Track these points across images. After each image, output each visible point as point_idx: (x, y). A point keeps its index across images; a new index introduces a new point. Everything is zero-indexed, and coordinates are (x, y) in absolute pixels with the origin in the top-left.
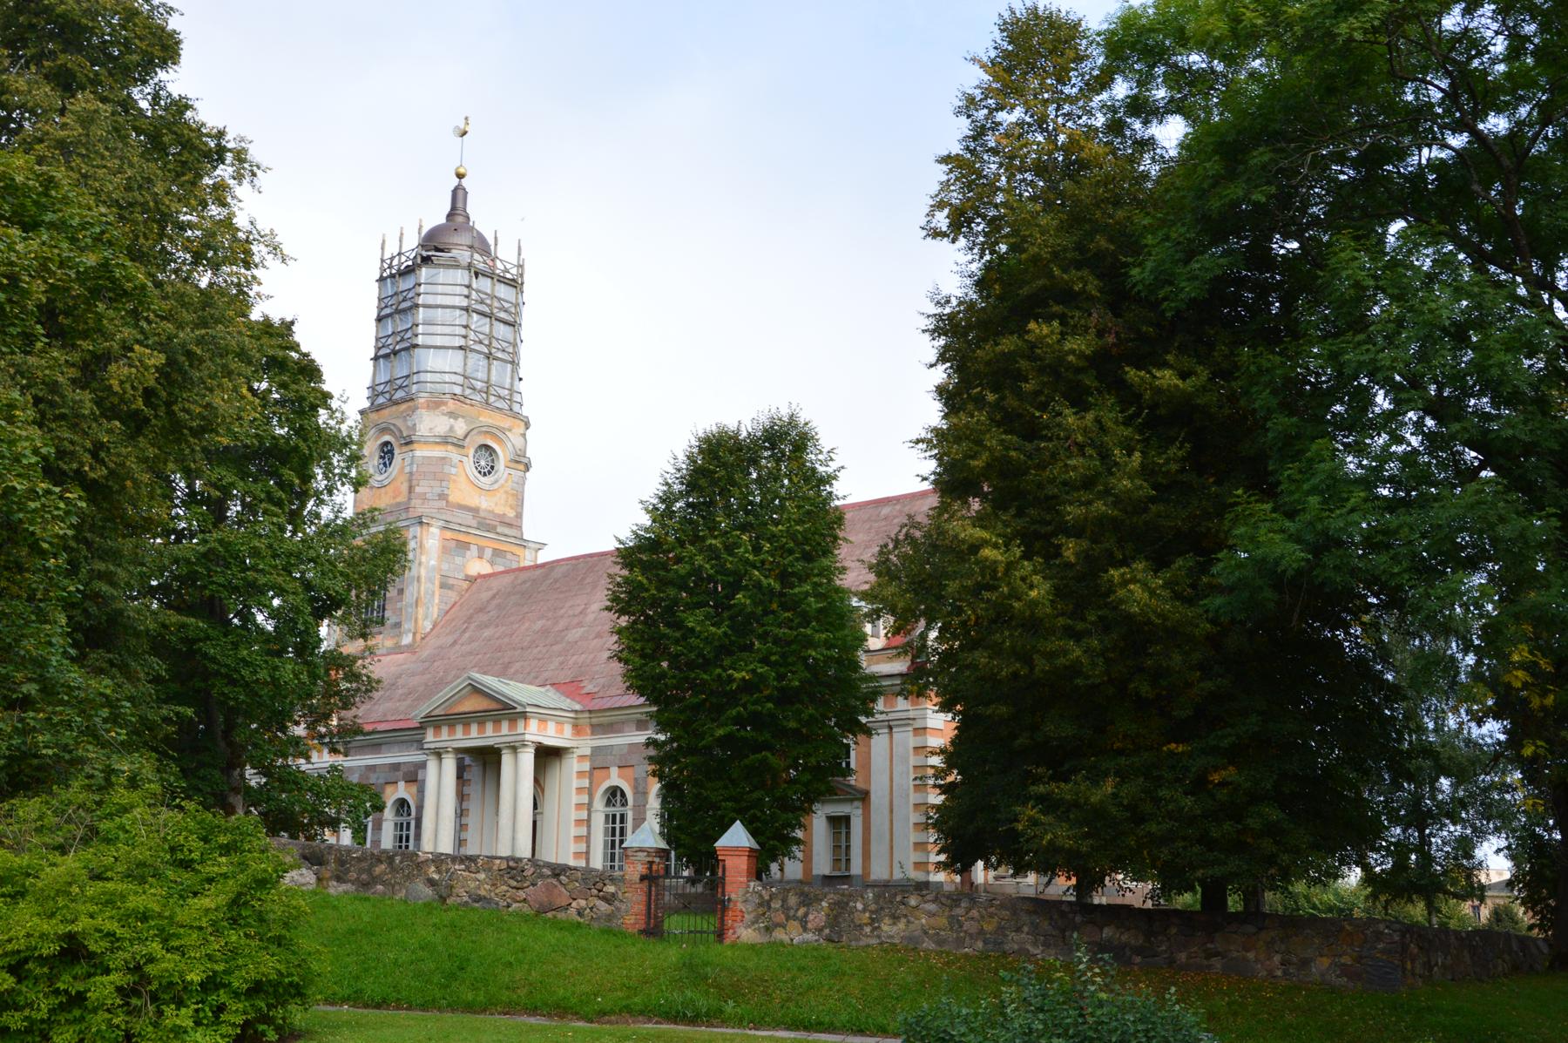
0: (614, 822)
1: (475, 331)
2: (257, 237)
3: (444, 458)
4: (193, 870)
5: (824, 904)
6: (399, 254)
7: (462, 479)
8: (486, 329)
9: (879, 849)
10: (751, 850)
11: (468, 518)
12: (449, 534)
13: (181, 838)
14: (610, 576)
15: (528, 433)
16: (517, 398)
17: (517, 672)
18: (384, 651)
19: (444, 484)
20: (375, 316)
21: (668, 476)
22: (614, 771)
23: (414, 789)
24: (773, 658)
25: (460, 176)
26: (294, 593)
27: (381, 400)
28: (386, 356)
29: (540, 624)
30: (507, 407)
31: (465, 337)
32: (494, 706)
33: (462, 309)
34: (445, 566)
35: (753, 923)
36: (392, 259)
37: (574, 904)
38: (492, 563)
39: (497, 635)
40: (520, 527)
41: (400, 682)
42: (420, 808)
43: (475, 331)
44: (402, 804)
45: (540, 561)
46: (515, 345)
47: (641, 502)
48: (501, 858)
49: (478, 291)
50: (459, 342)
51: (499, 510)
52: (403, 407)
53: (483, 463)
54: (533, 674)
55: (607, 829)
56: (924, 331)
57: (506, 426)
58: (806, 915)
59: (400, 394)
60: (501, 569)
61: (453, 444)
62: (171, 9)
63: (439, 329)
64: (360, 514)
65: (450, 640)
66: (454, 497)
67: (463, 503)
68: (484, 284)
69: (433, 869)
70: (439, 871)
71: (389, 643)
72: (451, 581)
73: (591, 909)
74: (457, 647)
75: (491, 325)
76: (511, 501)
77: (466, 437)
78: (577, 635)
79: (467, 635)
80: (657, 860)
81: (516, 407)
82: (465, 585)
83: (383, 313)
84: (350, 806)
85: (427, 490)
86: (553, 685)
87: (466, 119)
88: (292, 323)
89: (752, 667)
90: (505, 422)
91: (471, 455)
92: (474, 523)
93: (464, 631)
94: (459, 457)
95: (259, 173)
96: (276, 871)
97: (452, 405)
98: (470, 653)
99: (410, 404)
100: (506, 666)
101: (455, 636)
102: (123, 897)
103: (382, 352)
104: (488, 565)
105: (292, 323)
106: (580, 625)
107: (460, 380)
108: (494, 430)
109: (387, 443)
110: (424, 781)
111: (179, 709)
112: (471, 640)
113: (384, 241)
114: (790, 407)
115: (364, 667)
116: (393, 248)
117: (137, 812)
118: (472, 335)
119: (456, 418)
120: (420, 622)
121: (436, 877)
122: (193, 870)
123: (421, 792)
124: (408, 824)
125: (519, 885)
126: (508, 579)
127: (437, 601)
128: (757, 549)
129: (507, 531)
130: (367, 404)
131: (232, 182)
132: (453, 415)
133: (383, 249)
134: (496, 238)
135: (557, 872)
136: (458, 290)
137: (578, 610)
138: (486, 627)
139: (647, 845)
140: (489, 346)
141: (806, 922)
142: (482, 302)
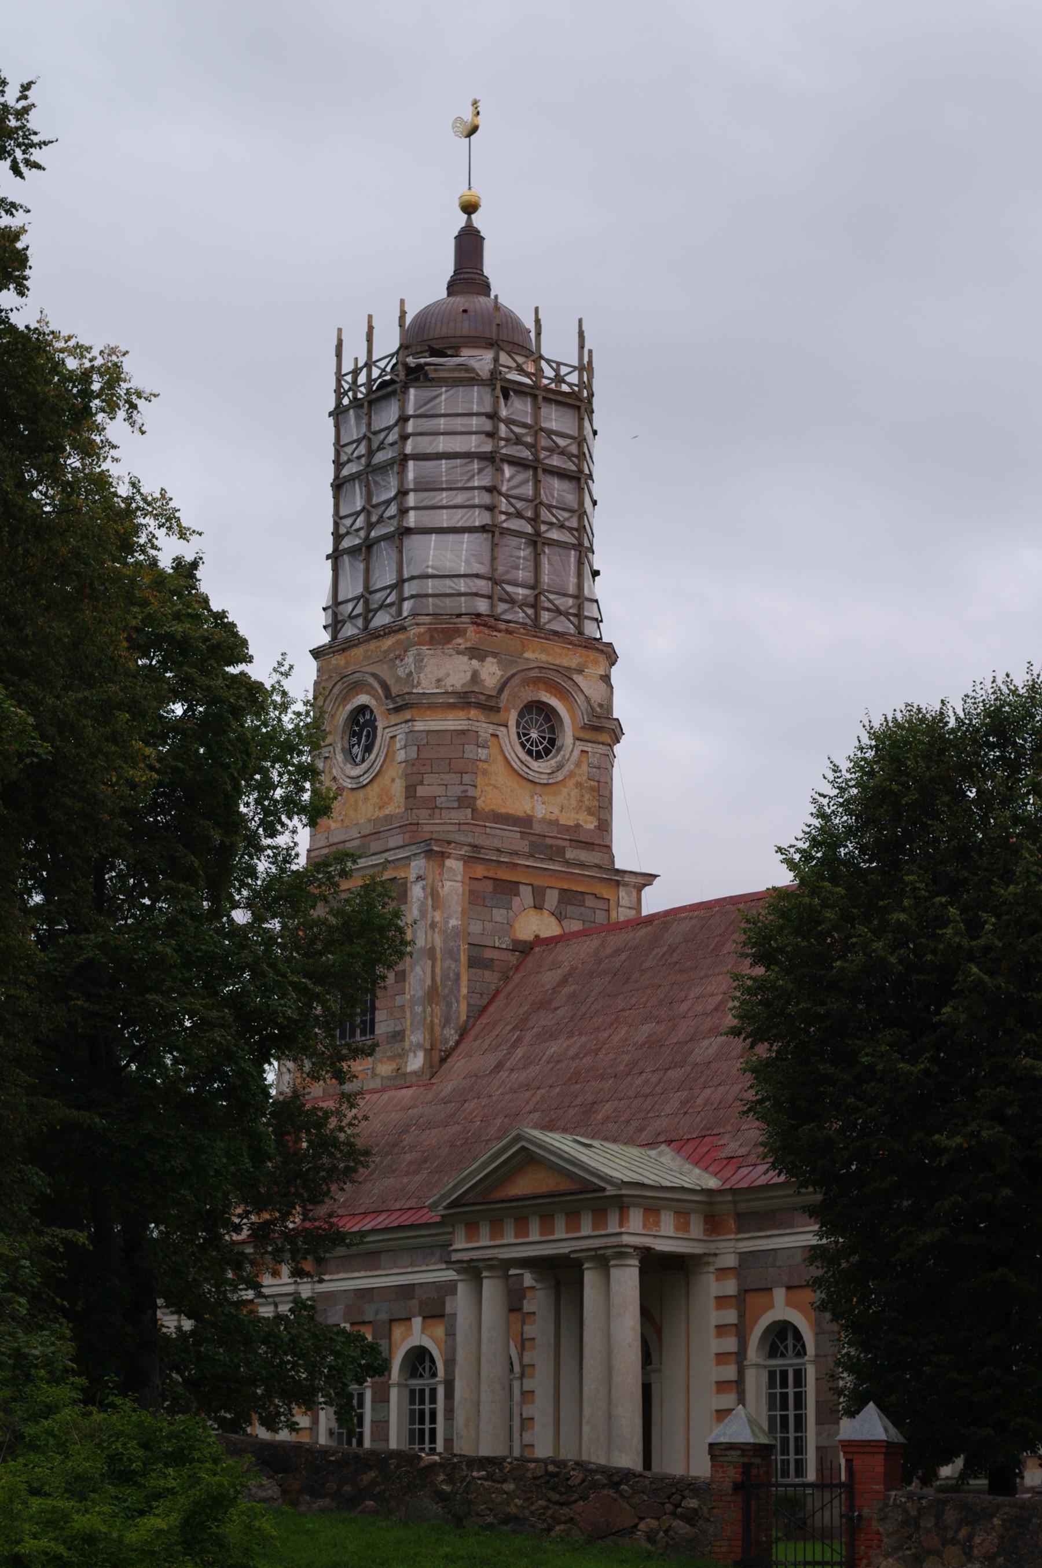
0: (784, 1384)
1: (507, 496)
2: (141, 504)
3: (463, 732)
4: (136, 1483)
5: (996, 1521)
6: (369, 365)
7: (498, 768)
8: (528, 490)
10: (888, 1445)
11: (511, 838)
12: (480, 871)
13: (119, 1445)
14: (736, 977)
15: (615, 672)
16: (590, 610)
17: (606, 1120)
18: (376, 1084)
19: (467, 778)
20: (330, 477)
21: (825, 801)
22: (779, 1294)
23: (440, 1331)
24: (1009, 1112)
25: (469, 208)
26: (222, 1026)
27: (349, 630)
28: (353, 551)
29: (646, 1029)
30: (572, 630)
31: (491, 508)
32: (566, 1185)
33: (482, 457)
34: (476, 928)
35: (896, 1550)
36: (356, 372)
37: (642, 1526)
38: (559, 916)
39: (572, 1052)
41: (408, 1139)
42: (450, 1363)
43: (507, 496)
44: (419, 1359)
45: (645, 911)
46: (581, 514)
47: (780, 850)
48: (536, 1461)
49: (509, 422)
50: (480, 518)
52: (389, 642)
53: (534, 735)
54: (635, 1124)
55: (771, 1397)
57: (573, 664)
58: (970, 1537)
59: (382, 619)
60: (576, 926)
61: (479, 706)
62: (13, 205)
63: (444, 497)
64: (318, 864)
65: (491, 1060)
66: (488, 800)
67: (502, 810)
68: (520, 408)
69: (442, 1477)
70: (450, 1480)
71: (385, 1069)
72: (488, 954)
73: (666, 1531)
74: (503, 1074)
75: (537, 483)
76: (588, 800)
77: (501, 690)
79: (519, 1053)
80: (757, 1461)
81: (590, 629)
82: (513, 959)
83: (345, 472)
84: (331, 1368)
85: (438, 791)
86: (669, 1142)
87: (475, 103)
88: (194, 565)
89: (973, 1127)
90: (571, 659)
91: (512, 723)
92: (523, 846)
93: (515, 1045)
95: (141, 403)
96: (234, 1486)
97: (472, 635)
98: (528, 1086)
99: (401, 636)
100: (589, 1109)
101: (500, 1055)
102: (65, 1517)
103: (346, 543)
105: (194, 565)
107: (483, 586)
108: (552, 675)
109: (363, 709)
110: (454, 1315)
111: (65, 1233)
113: (371, 328)
114: (1029, 671)
115: (341, 1129)
116: (355, 352)
117: (67, 1413)
118: (503, 504)
119: (482, 659)
120: (438, 1029)
121: (446, 1488)
122: (136, 1483)
123: (451, 1333)
124: (433, 1391)
125: (563, 1499)
126: (587, 947)
127: (464, 991)
128: (974, 928)
129: (583, 856)
130: (324, 638)
131: (147, 610)
132: (476, 653)
133: (339, 354)
134: (538, 321)
135: (616, 1479)
136: (474, 423)
138: (553, 1036)
139: (741, 1439)
140: (535, 520)
141: (971, 1547)
142: (518, 441)
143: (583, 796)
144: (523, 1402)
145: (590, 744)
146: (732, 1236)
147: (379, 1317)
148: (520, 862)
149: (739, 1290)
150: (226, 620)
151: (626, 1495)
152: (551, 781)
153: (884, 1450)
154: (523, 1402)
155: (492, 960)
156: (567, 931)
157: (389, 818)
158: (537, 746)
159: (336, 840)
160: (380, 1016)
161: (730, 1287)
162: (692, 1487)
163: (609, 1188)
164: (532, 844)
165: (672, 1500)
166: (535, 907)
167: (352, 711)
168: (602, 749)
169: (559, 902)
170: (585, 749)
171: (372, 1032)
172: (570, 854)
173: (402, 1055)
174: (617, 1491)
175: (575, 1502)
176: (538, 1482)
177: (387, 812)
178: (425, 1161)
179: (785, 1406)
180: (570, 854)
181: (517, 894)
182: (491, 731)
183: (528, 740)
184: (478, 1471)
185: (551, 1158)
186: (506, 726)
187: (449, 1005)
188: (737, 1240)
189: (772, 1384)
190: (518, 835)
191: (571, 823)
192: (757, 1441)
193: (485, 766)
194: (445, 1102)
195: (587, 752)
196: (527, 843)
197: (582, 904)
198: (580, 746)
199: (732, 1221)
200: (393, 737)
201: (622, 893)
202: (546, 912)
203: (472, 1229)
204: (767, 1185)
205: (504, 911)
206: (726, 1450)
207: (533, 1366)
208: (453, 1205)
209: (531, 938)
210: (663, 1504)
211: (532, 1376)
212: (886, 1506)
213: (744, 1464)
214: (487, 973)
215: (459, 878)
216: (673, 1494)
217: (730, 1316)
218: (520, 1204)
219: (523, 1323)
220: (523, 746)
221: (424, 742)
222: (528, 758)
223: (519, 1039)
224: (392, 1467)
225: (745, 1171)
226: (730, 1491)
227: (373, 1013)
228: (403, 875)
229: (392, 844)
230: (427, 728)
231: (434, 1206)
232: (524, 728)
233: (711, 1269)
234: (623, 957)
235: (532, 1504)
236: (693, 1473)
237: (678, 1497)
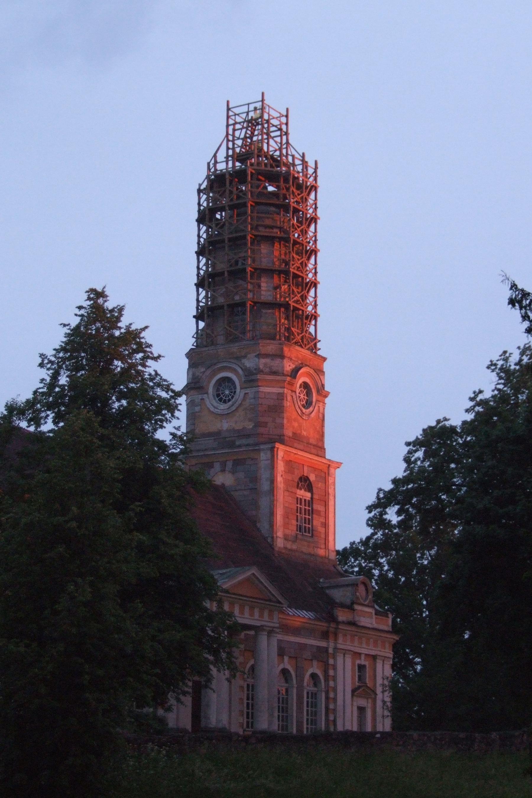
38: (233, 472)
51: (238, 427)
94: (200, 397)
145: (248, 389)
148: (209, 453)
150: (131, 329)
158: (224, 396)
169: (233, 465)
170: (246, 392)
172: (238, 443)
180: (238, 443)
182: (200, 398)
183: (231, 389)
191: (241, 428)
195: (248, 393)
196: (217, 443)
198: (244, 391)
202: (227, 472)
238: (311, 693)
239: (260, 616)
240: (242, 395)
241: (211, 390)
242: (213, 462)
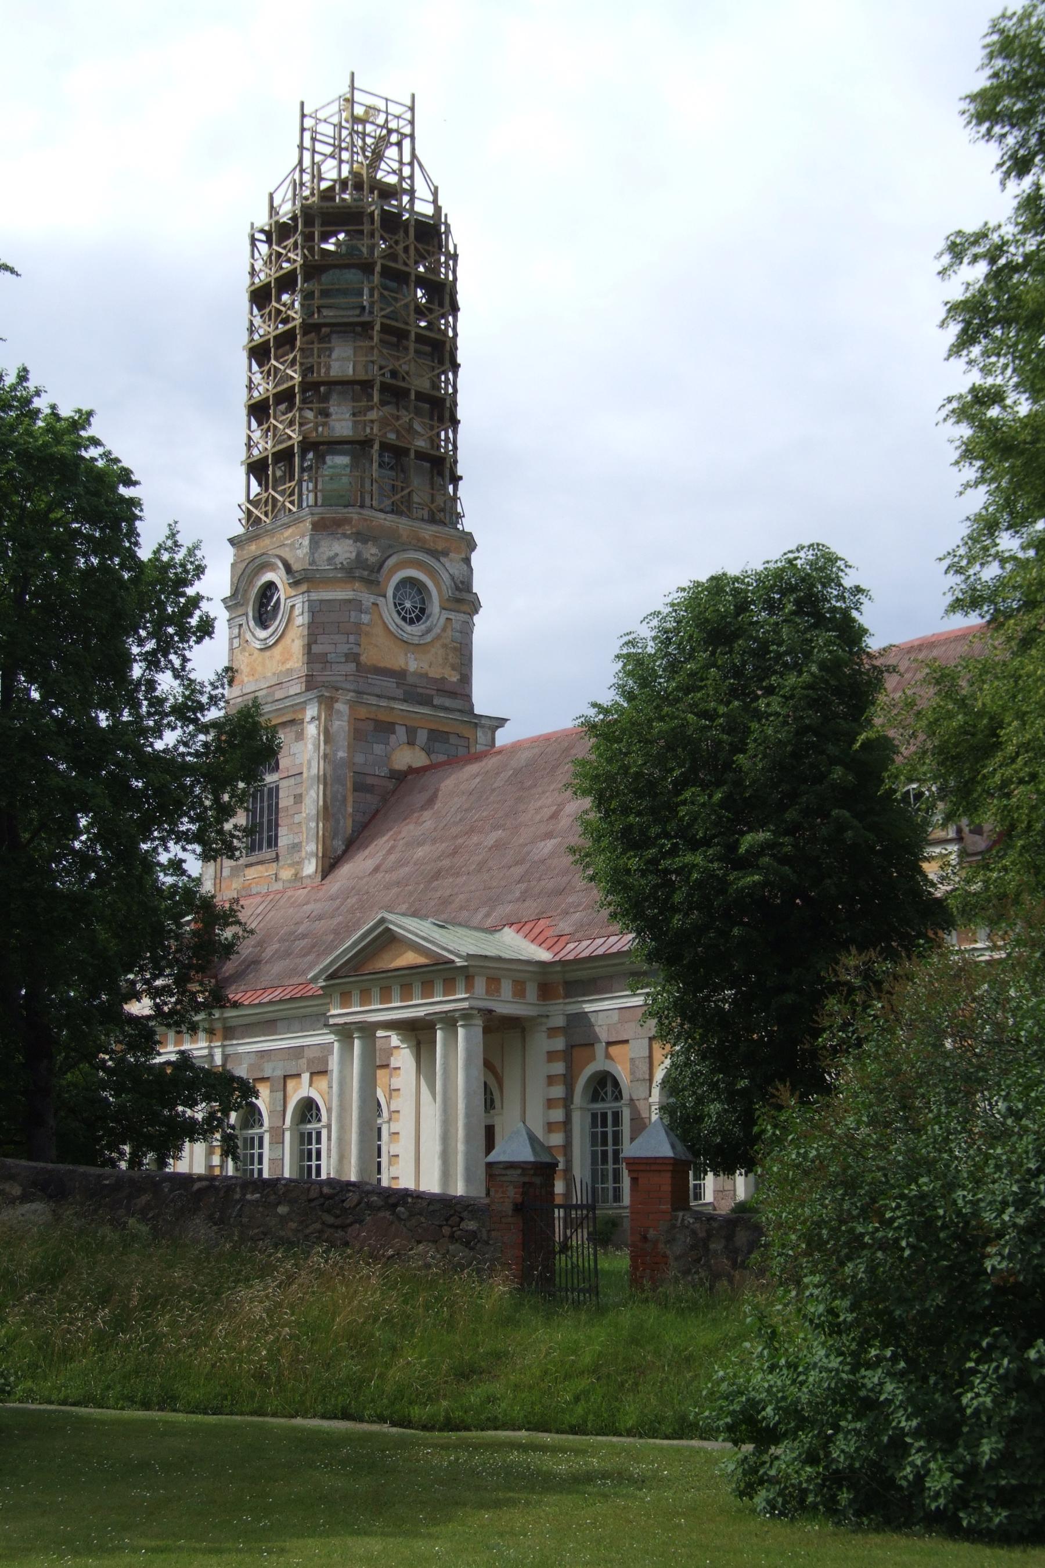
0: (604, 1124)
3: (349, 601)
9: (404, 1147)
34: (360, 759)
38: (428, 752)
40: (468, 697)
51: (435, 673)
53: (408, 605)
55: (594, 1136)
56: (947, 359)
60: (442, 758)
67: (382, 665)
72: (370, 781)
74: (379, 876)
76: (452, 658)
78: (546, 851)
79: (392, 858)
80: (537, 1180)
82: (390, 785)
92: (399, 693)
94: (372, 599)
98: (398, 884)
104: (423, 754)
106: (549, 835)
112: (400, 863)
125: (338, 1222)
127: (350, 810)
129: (448, 702)
135: (392, 1200)
137: (547, 812)
138: (421, 844)
143: (447, 655)
144: (391, 1142)
146: (561, 1001)
147: (275, 1074)
149: (567, 1046)
151: (403, 1217)
152: (422, 642)
153: (671, 1168)
154: (391, 1142)
155: (373, 785)
156: (434, 762)
157: (290, 671)
159: (249, 691)
160: (282, 831)
161: (559, 1044)
162: (470, 1208)
163: (457, 960)
164: (405, 693)
165: (450, 1222)
166: (408, 743)
167: (261, 587)
168: (462, 617)
169: (428, 739)
171: (276, 845)
172: (436, 702)
173: (299, 863)
174: (394, 1213)
175: (351, 1225)
176: (312, 1205)
177: (288, 666)
178: (313, 946)
179: (605, 1143)
180: (436, 702)
181: (394, 733)
182: (372, 600)
183: (402, 609)
184: (253, 1193)
185: (410, 936)
186: (385, 596)
187: (337, 821)
188: (565, 1004)
189: (594, 1124)
190: (395, 685)
191: (438, 677)
192: (539, 1159)
193: (368, 629)
194: (332, 898)
197: (447, 741)
198: (445, 615)
199: (561, 988)
200: (293, 606)
201: (480, 733)
203: (345, 999)
204: (589, 957)
205: (383, 746)
206: (506, 1168)
207: (398, 1112)
208: (331, 977)
209: (405, 768)
210: (441, 1226)
211: (398, 1120)
212: (674, 1227)
213: (524, 1183)
214: (368, 796)
215: (346, 718)
216: (451, 1216)
217: (559, 1068)
218: (384, 975)
219: (391, 1076)
220: (399, 613)
221: (318, 609)
222: (403, 623)
223: (393, 848)
224: (166, 1190)
225: (571, 946)
226: (510, 1213)
227: (276, 830)
228: (300, 717)
229: (292, 692)
230: (320, 598)
231: (315, 979)
232: (400, 599)
233: (544, 1028)
234: (478, 780)
235: (307, 1227)
236: (422, 1189)
237: (456, 1219)
238: (613, 1113)
239: (515, 995)
240: (442, 620)
241: (390, 593)
242: (393, 724)
